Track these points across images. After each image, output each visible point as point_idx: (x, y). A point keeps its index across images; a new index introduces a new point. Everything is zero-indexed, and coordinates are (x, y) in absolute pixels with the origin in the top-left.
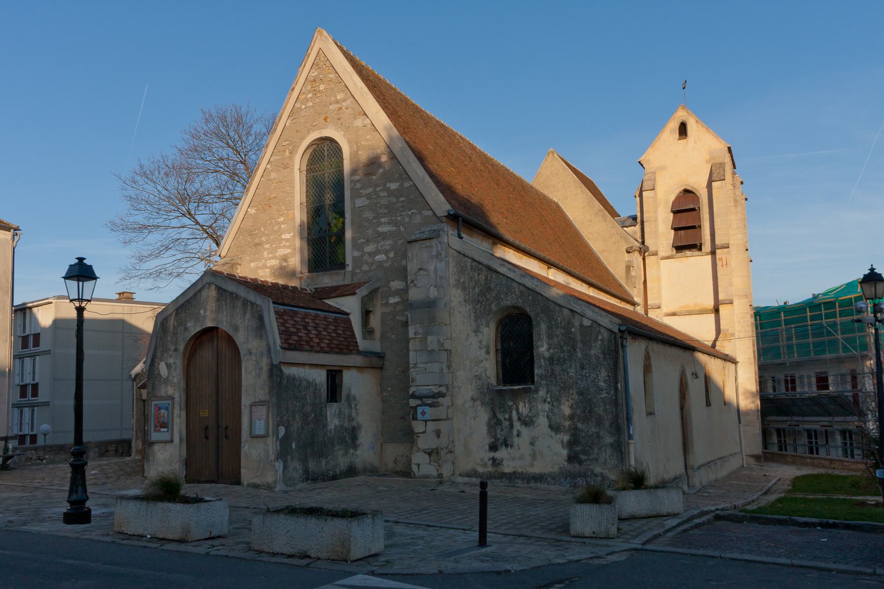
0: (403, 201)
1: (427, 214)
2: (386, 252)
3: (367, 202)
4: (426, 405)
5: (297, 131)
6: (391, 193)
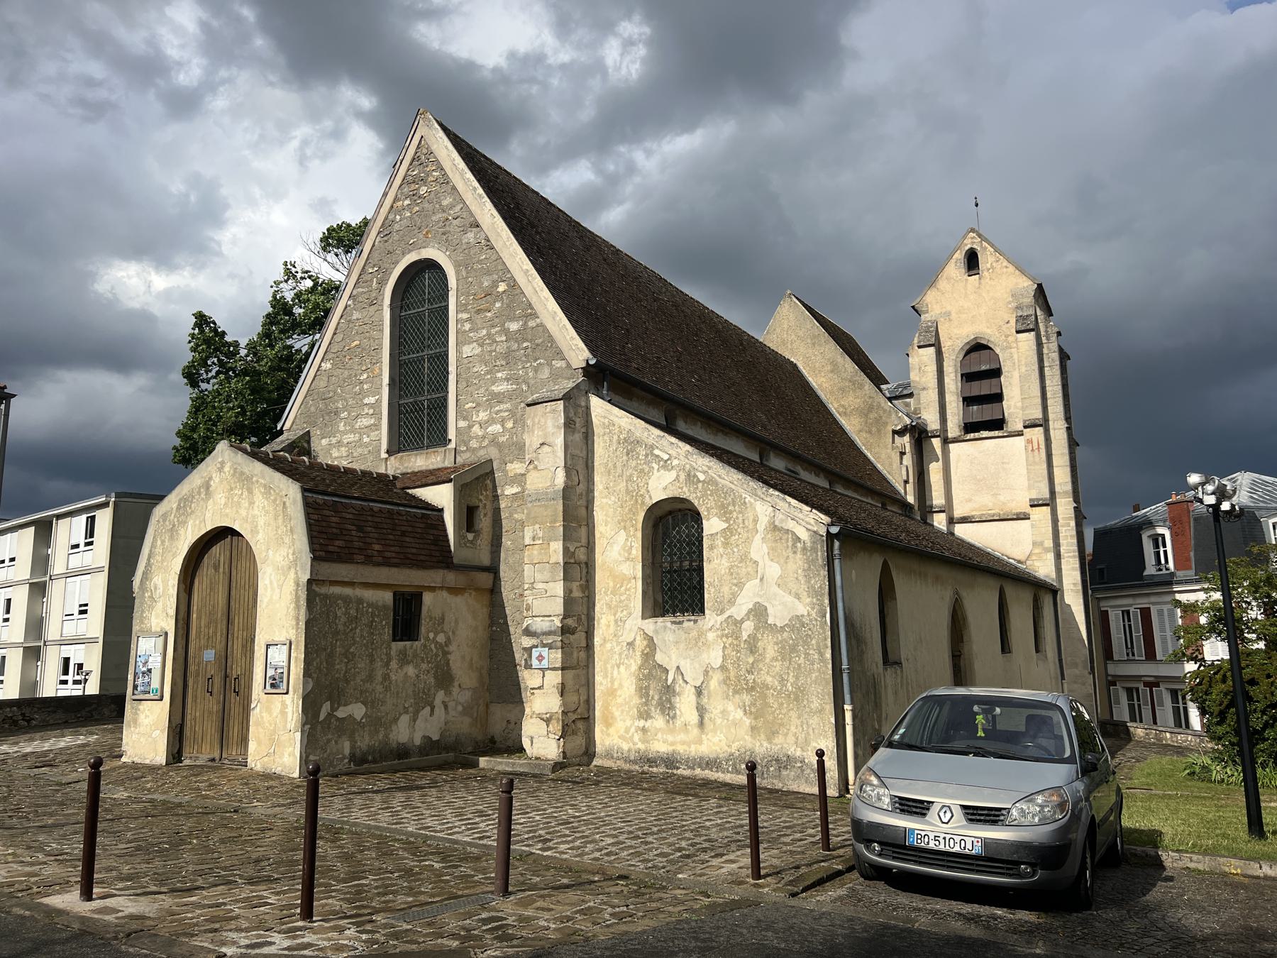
0: (526, 348)
1: (558, 365)
2: (503, 422)
3: (478, 350)
4: (544, 646)
5: (389, 253)
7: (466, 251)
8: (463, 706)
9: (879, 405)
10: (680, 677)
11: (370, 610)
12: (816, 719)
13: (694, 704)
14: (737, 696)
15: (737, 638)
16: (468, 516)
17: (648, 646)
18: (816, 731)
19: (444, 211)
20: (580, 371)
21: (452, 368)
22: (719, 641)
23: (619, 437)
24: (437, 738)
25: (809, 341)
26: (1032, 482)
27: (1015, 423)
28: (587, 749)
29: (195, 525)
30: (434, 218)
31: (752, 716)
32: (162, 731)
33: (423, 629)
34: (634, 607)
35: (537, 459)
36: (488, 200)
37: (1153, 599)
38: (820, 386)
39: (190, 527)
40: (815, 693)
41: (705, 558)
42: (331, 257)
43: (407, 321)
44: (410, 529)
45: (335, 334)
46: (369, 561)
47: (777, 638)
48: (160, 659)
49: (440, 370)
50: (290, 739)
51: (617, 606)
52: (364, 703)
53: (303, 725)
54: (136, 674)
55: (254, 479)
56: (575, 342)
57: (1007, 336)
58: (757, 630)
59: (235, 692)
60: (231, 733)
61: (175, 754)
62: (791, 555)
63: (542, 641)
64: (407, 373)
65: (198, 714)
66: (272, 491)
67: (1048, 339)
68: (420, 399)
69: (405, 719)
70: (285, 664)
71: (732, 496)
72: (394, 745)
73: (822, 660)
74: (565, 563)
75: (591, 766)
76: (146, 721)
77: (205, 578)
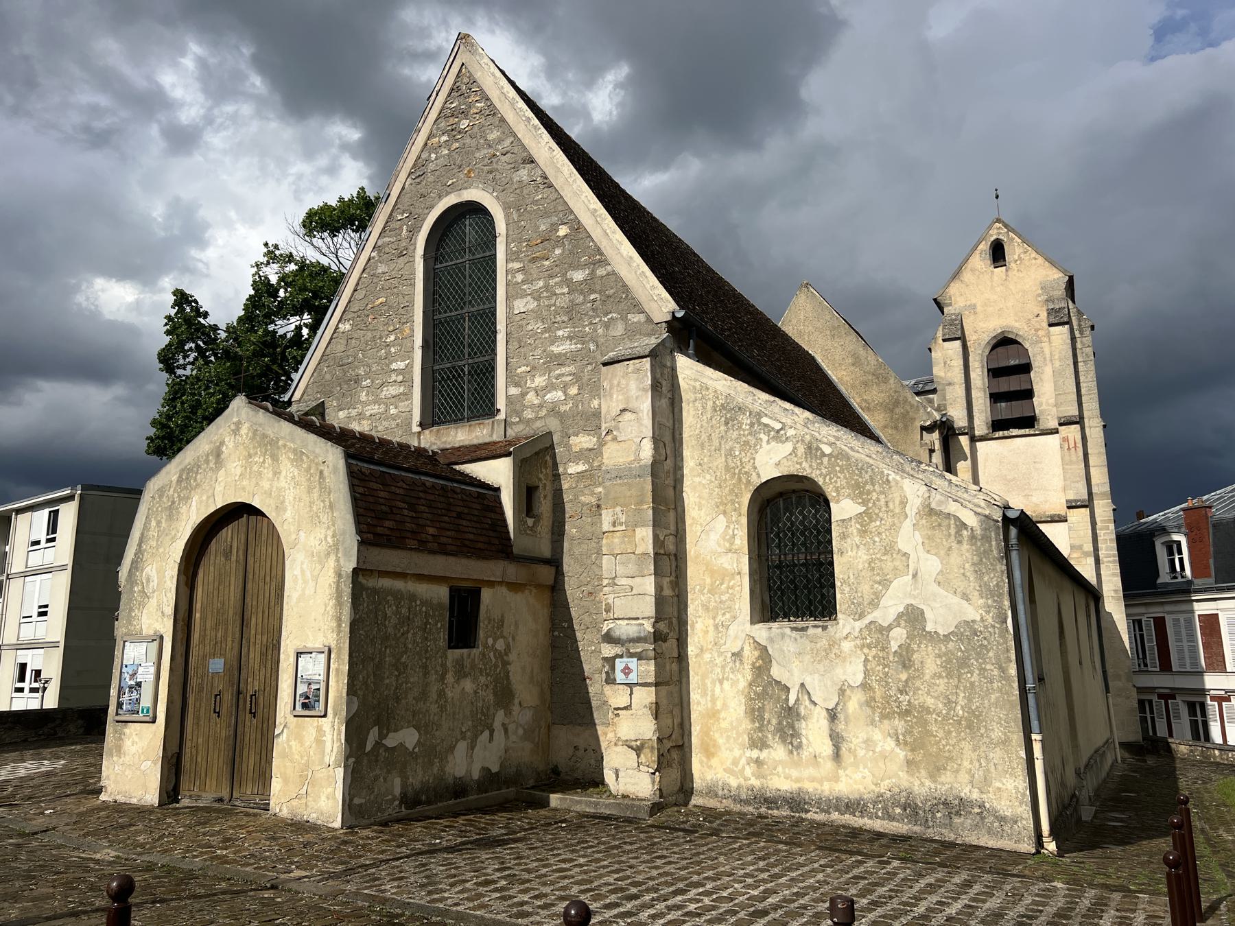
0: (594, 301)
1: (635, 320)
2: (565, 388)
3: (533, 305)
4: (631, 655)
5: (423, 196)
6: (573, 287)
7: (518, 191)
8: (524, 729)
9: (905, 400)
10: (806, 697)
11: (424, 609)
12: (998, 752)
13: (826, 732)
14: (886, 722)
15: (883, 649)
16: (527, 495)
17: (760, 657)
18: (1000, 768)
19: (490, 146)
20: (664, 325)
21: (501, 326)
22: (859, 652)
23: (714, 403)
24: (497, 770)
25: (828, 333)
26: (1068, 482)
27: (1048, 419)
28: (682, 786)
29: (201, 502)
30: (477, 155)
31: (908, 748)
32: (154, 762)
33: (481, 634)
34: (740, 609)
35: (617, 428)
36: (546, 132)
37: (1168, 608)
38: (841, 379)
39: (194, 503)
41: (835, 549)
42: (317, 241)
43: (443, 274)
44: (466, 511)
45: (355, 290)
46: (423, 547)
47: (940, 649)
48: (152, 670)
49: (484, 330)
50: (329, 777)
51: (716, 608)
52: (417, 728)
53: (347, 759)
54: (120, 689)
55: (281, 443)
56: (657, 292)
57: (1037, 330)
58: (912, 640)
59: (251, 713)
60: (244, 766)
61: (171, 791)
62: (954, 545)
63: (628, 650)
64: (443, 334)
65: (200, 740)
66: (304, 458)
67: (1081, 333)
68: (460, 363)
69: (462, 746)
70: (322, 678)
71: (870, 473)
72: (450, 780)
74: (656, 554)
75: (690, 806)
76: (134, 749)
77: (212, 568)
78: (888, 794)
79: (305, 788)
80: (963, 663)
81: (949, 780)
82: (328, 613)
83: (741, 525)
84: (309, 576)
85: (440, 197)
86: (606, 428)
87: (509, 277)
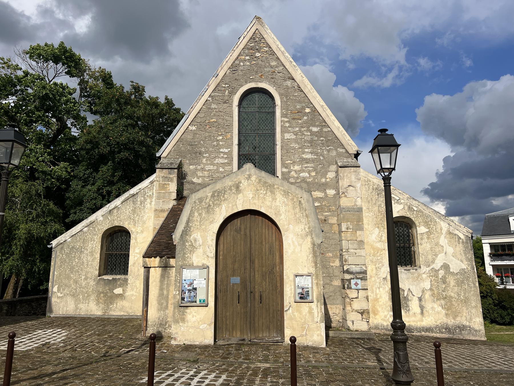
0: (322, 140)
1: (341, 151)
2: (309, 172)
3: (294, 137)
6: (312, 133)
7: (285, 89)
10: (411, 293)
14: (438, 301)
15: (437, 277)
20: (353, 155)
31: (446, 310)
35: (347, 192)
40: (473, 300)
50: (317, 327)
55: (275, 187)
56: (350, 142)
71: (430, 218)
73: (475, 286)
77: (229, 237)
78: (440, 325)
79: (305, 332)
80: (463, 282)
81: (459, 319)
82: (309, 259)
83: (385, 232)
84: (297, 244)
85: (246, 82)
86: (342, 192)
87: (282, 124)
